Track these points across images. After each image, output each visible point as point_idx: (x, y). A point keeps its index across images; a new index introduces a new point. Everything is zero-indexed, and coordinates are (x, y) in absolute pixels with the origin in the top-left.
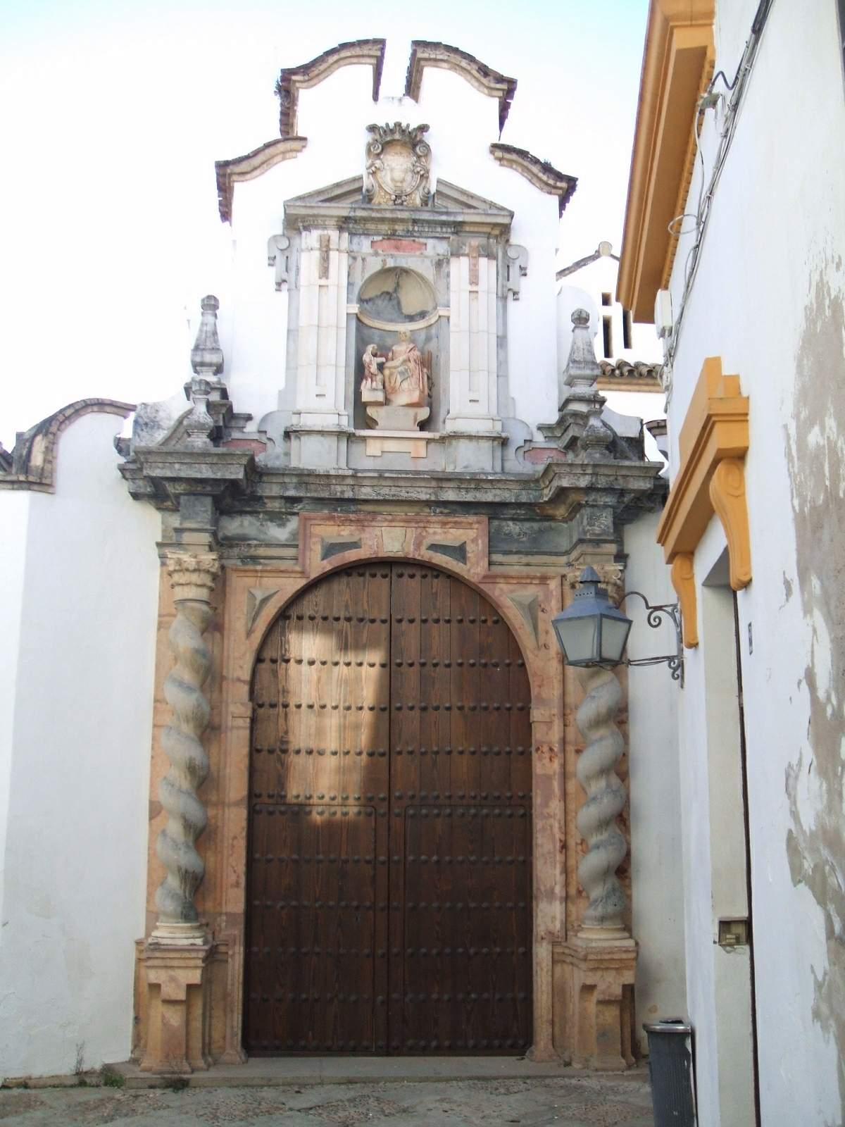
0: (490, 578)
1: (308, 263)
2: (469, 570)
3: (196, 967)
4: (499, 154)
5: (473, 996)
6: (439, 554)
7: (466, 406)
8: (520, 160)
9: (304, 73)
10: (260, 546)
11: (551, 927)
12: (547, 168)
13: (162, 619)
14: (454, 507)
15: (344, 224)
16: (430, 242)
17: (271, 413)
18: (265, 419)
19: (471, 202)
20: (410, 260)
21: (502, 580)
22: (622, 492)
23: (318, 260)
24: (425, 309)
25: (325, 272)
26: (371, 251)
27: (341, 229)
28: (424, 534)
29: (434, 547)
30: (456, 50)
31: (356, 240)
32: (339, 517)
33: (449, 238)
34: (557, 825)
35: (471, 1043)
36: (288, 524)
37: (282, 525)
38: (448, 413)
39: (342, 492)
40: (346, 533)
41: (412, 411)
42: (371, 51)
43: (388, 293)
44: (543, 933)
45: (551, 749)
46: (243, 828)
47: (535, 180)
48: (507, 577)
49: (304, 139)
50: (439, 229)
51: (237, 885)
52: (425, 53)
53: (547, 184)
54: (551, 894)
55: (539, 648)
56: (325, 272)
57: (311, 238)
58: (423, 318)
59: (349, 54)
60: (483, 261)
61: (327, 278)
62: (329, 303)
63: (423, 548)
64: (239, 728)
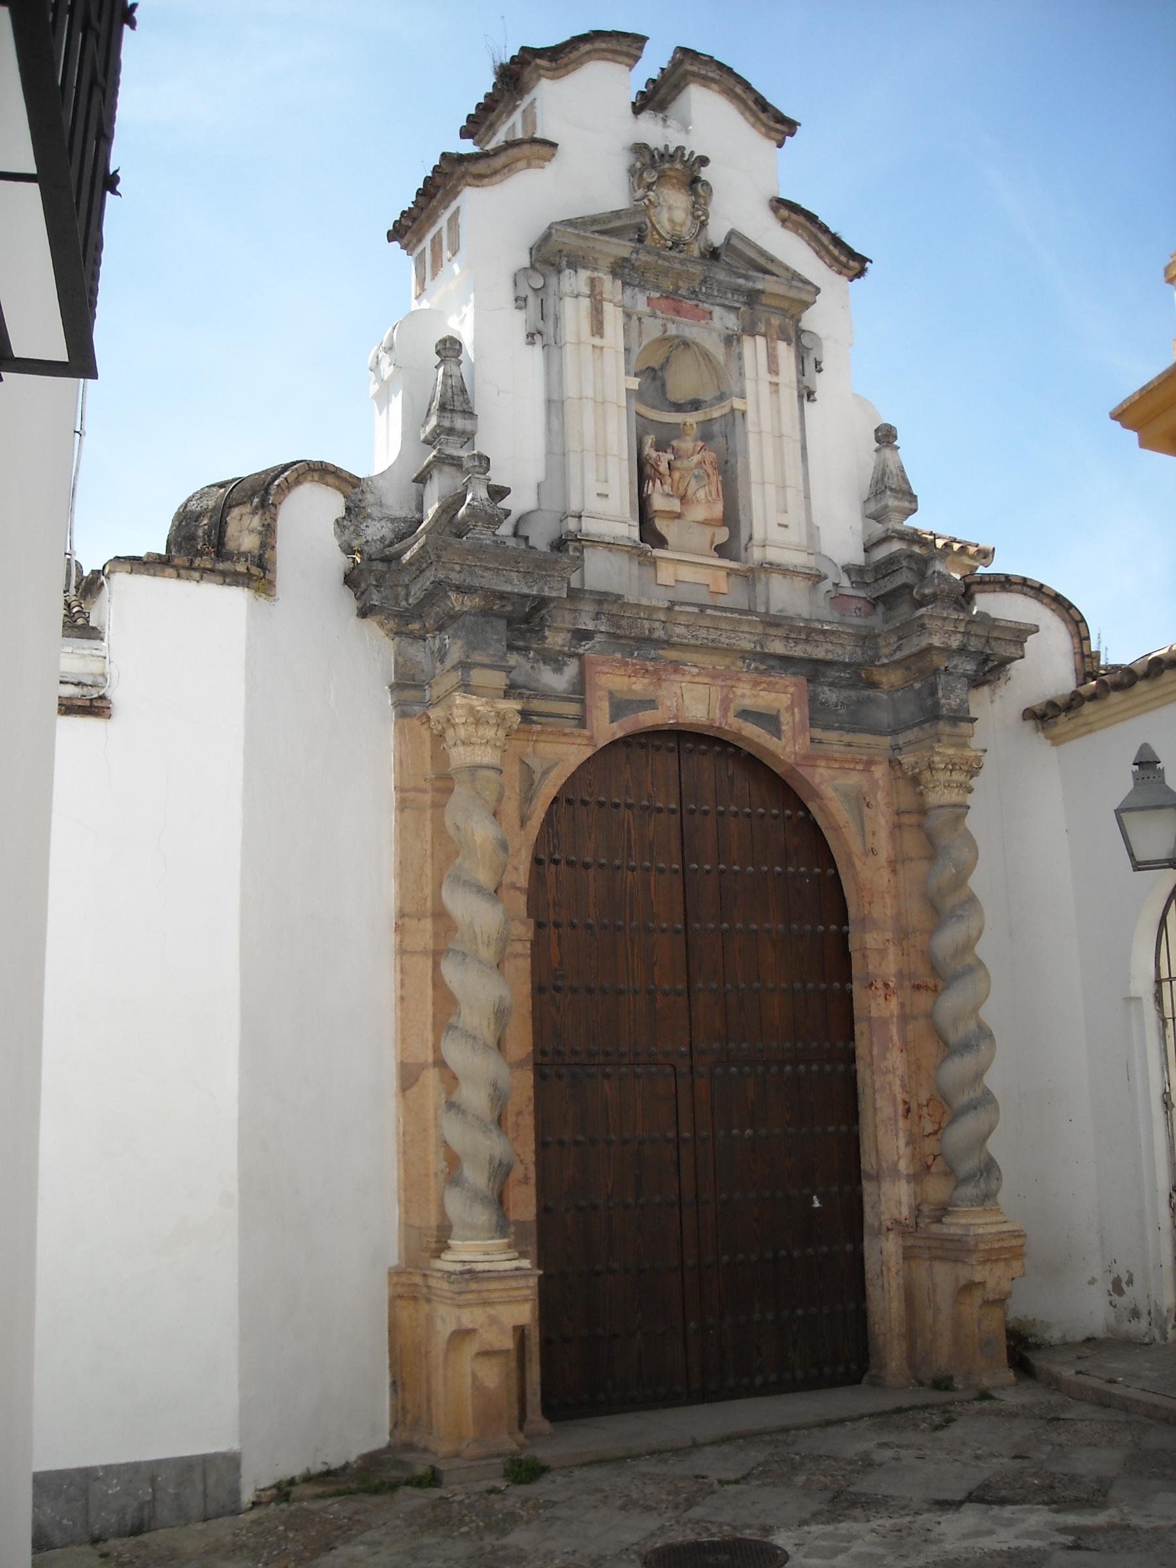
0: (809, 760)
1: (574, 315)
2: (784, 748)
3: (526, 1300)
4: (784, 212)
5: (800, 1312)
6: (749, 724)
7: (772, 529)
8: (808, 225)
9: (552, 59)
10: (536, 697)
11: (896, 1215)
12: (837, 241)
13: (406, 795)
14: (773, 663)
15: (620, 269)
16: (717, 311)
17: (528, 513)
18: (522, 519)
19: (770, 267)
20: (694, 330)
21: (823, 763)
22: (987, 659)
23: (589, 310)
24: (702, 398)
25: (598, 328)
26: (647, 310)
27: (614, 274)
28: (731, 696)
29: (745, 714)
30: (729, 71)
31: (629, 291)
32: (633, 665)
33: (739, 309)
34: (898, 1082)
35: (799, 1374)
36: (566, 668)
37: (559, 669)
38: (751, 538)
39: (651, 630)
40: (639, 686)
41: (708, 531)
42: (624, 45)
43: (653, 370)
44: (889, 1224)
45: (886, 985)
46: (530, 1100)
47: (823, 253)
48: (828, 758)
49: (554, 145)
50: (729, 296)
51: (526, 1180)
52: (689, 67)
53: (836, 260)
54: (895, 1174)
55: (866, 853)
56: (598, 328)
57: (576, 281)
58: (697, 409)
59: (603, 46)
60: (782, 346)
61: (602, 337)
62: (603, 376)
63: (731, 714)
64: (517, 956)
